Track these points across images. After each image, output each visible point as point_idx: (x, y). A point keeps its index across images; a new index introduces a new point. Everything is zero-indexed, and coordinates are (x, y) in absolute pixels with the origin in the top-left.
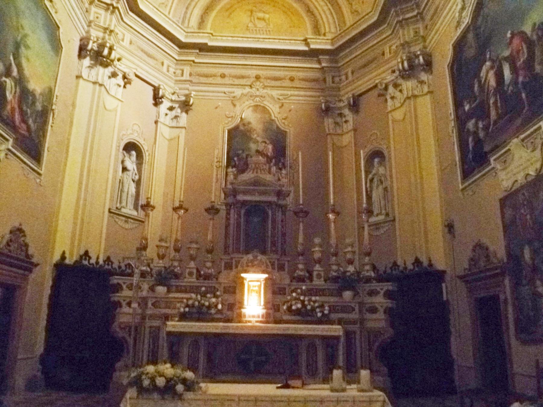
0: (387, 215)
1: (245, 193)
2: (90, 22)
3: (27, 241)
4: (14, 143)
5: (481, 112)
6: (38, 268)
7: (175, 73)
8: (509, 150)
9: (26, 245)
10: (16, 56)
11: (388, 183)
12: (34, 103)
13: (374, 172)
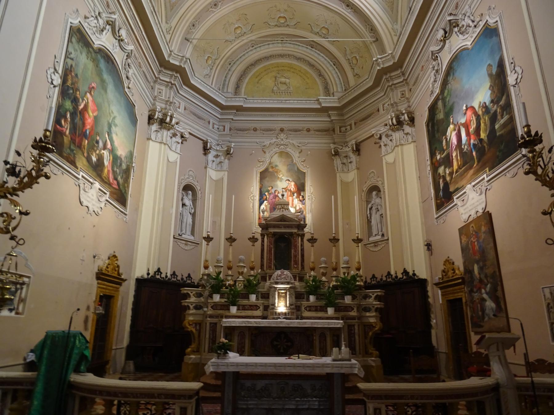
0: (383, 235)
1: (275, 226)
2: (155, 97)
3: (119, 263)
4: (110, 195)
5: (448, 161)
6: (126, 282)
7: (218, 129)
8: (465, 192)
9: (118, 266)
10: (109, 134)
11: (382, 211)
12: (121, 165)
13: (373, 202)
